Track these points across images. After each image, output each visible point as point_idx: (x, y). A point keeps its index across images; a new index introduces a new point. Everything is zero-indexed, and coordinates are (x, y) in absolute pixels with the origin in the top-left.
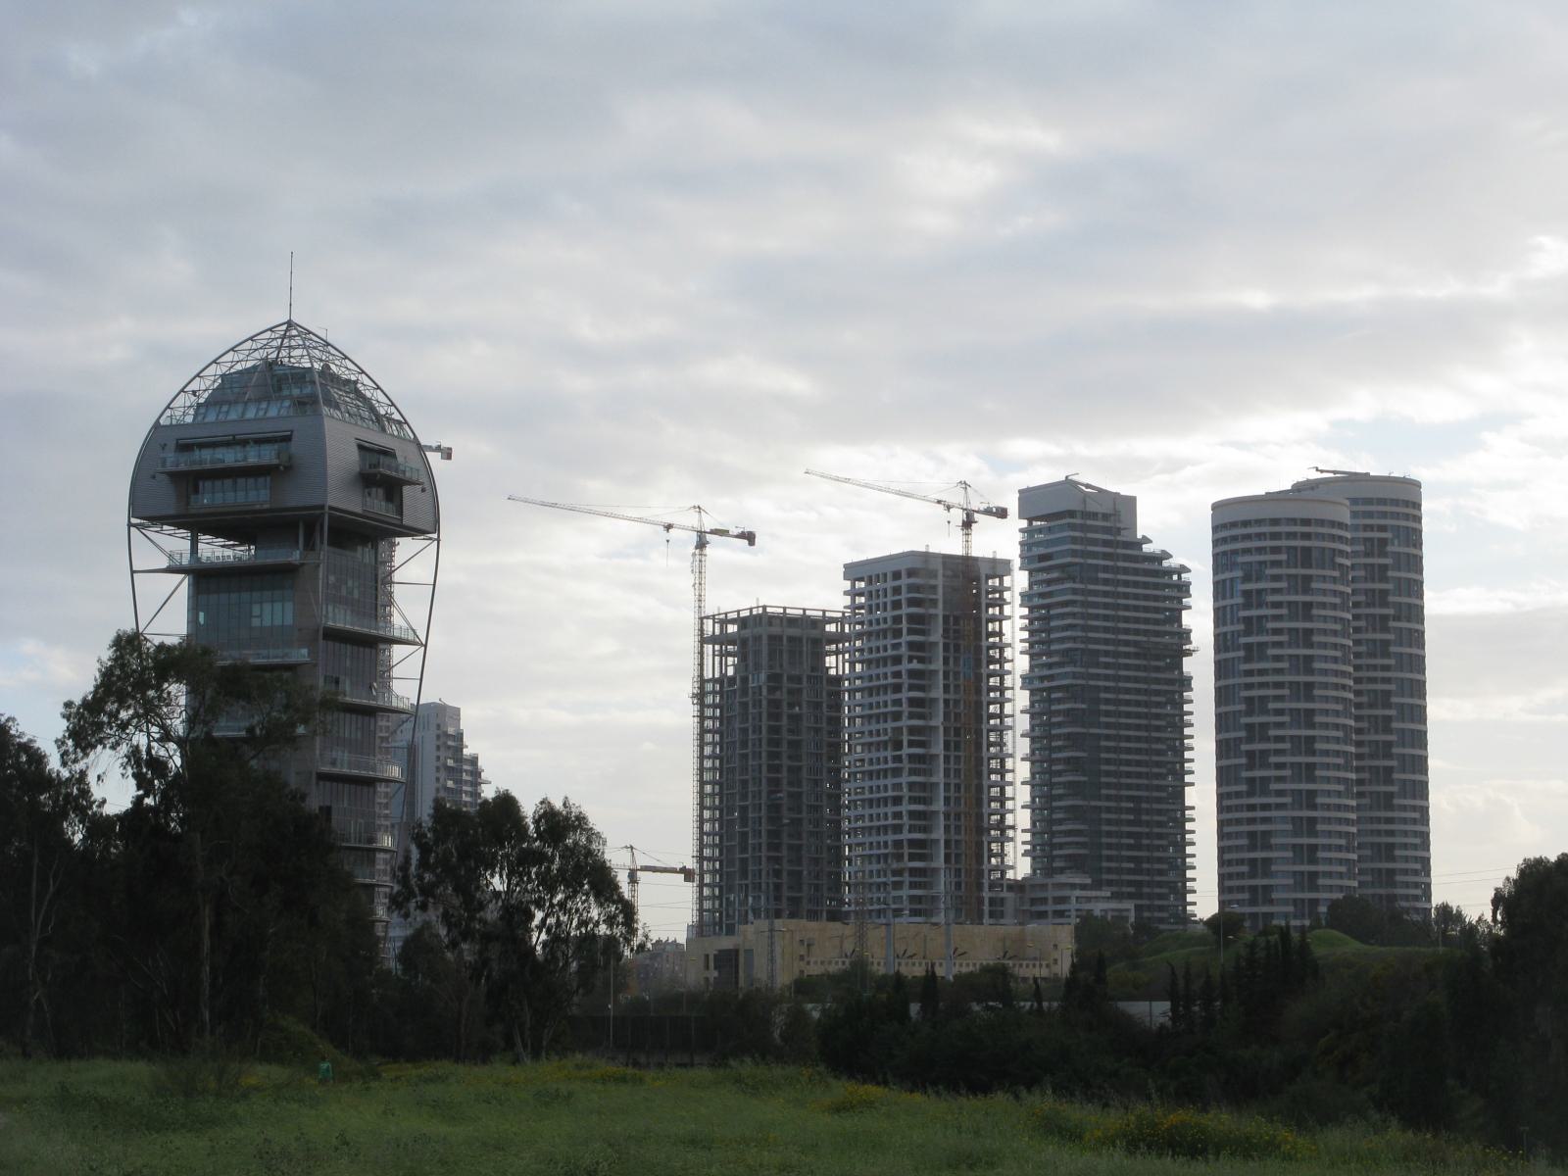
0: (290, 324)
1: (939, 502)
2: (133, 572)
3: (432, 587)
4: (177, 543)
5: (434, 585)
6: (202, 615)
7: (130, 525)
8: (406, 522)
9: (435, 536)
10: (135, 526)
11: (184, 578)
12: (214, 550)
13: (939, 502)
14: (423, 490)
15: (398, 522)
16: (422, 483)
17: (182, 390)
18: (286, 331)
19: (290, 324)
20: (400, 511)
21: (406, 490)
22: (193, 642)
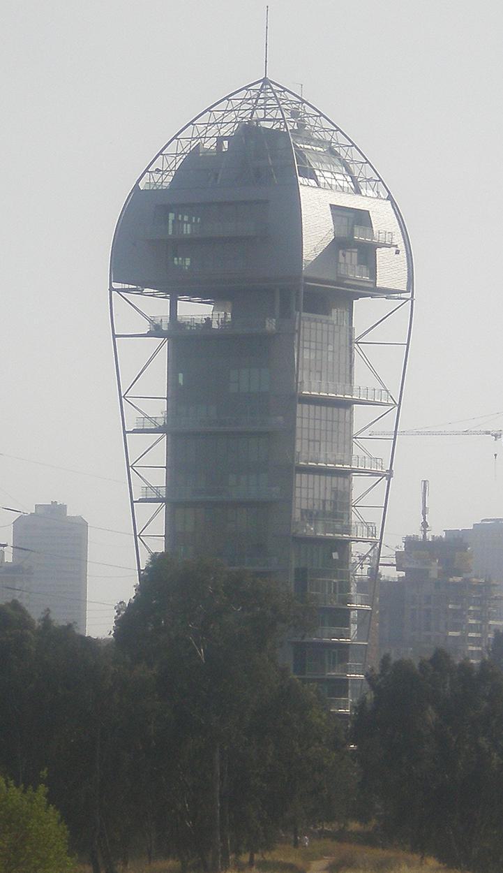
0: (265, 81)
1: (488, 433)
2: (115, 336)
3: (406, 346)
4: (157, 306)
5: (408, 345)
6: (181, 375)
7: (111, 289)
8: (379, 284)
9: (408, 295)
10: (115, 290)
11: (161, 345)
12: (195, 311)
13: (488, 433)
14: (397, 252)
15: (371, 286)
16: (396, 246)
17: (146, 171)
18: (262, 86)
19: (265, 81)
20: (373, 275)
21: (380, 252)
22: (368, 231)
